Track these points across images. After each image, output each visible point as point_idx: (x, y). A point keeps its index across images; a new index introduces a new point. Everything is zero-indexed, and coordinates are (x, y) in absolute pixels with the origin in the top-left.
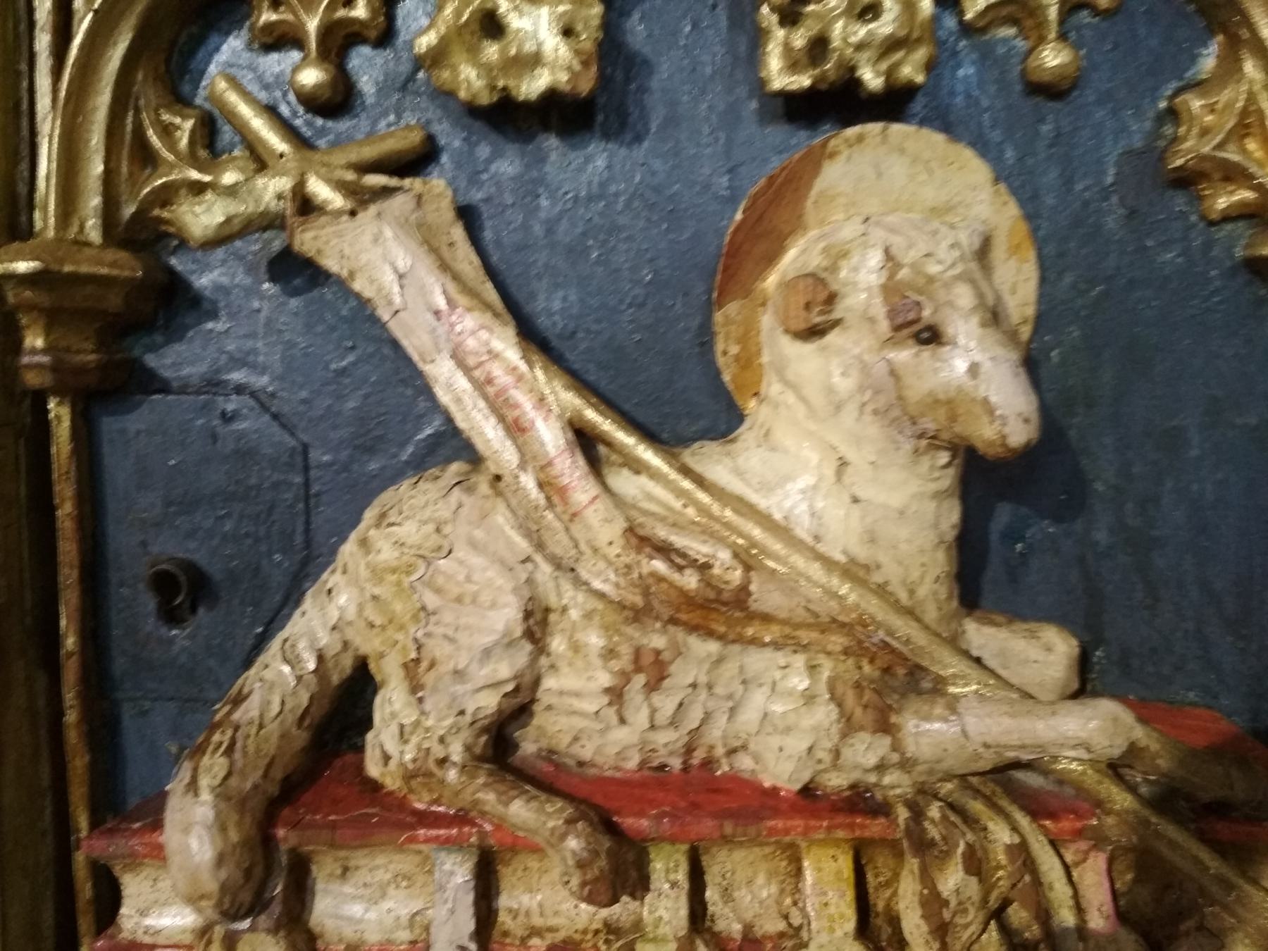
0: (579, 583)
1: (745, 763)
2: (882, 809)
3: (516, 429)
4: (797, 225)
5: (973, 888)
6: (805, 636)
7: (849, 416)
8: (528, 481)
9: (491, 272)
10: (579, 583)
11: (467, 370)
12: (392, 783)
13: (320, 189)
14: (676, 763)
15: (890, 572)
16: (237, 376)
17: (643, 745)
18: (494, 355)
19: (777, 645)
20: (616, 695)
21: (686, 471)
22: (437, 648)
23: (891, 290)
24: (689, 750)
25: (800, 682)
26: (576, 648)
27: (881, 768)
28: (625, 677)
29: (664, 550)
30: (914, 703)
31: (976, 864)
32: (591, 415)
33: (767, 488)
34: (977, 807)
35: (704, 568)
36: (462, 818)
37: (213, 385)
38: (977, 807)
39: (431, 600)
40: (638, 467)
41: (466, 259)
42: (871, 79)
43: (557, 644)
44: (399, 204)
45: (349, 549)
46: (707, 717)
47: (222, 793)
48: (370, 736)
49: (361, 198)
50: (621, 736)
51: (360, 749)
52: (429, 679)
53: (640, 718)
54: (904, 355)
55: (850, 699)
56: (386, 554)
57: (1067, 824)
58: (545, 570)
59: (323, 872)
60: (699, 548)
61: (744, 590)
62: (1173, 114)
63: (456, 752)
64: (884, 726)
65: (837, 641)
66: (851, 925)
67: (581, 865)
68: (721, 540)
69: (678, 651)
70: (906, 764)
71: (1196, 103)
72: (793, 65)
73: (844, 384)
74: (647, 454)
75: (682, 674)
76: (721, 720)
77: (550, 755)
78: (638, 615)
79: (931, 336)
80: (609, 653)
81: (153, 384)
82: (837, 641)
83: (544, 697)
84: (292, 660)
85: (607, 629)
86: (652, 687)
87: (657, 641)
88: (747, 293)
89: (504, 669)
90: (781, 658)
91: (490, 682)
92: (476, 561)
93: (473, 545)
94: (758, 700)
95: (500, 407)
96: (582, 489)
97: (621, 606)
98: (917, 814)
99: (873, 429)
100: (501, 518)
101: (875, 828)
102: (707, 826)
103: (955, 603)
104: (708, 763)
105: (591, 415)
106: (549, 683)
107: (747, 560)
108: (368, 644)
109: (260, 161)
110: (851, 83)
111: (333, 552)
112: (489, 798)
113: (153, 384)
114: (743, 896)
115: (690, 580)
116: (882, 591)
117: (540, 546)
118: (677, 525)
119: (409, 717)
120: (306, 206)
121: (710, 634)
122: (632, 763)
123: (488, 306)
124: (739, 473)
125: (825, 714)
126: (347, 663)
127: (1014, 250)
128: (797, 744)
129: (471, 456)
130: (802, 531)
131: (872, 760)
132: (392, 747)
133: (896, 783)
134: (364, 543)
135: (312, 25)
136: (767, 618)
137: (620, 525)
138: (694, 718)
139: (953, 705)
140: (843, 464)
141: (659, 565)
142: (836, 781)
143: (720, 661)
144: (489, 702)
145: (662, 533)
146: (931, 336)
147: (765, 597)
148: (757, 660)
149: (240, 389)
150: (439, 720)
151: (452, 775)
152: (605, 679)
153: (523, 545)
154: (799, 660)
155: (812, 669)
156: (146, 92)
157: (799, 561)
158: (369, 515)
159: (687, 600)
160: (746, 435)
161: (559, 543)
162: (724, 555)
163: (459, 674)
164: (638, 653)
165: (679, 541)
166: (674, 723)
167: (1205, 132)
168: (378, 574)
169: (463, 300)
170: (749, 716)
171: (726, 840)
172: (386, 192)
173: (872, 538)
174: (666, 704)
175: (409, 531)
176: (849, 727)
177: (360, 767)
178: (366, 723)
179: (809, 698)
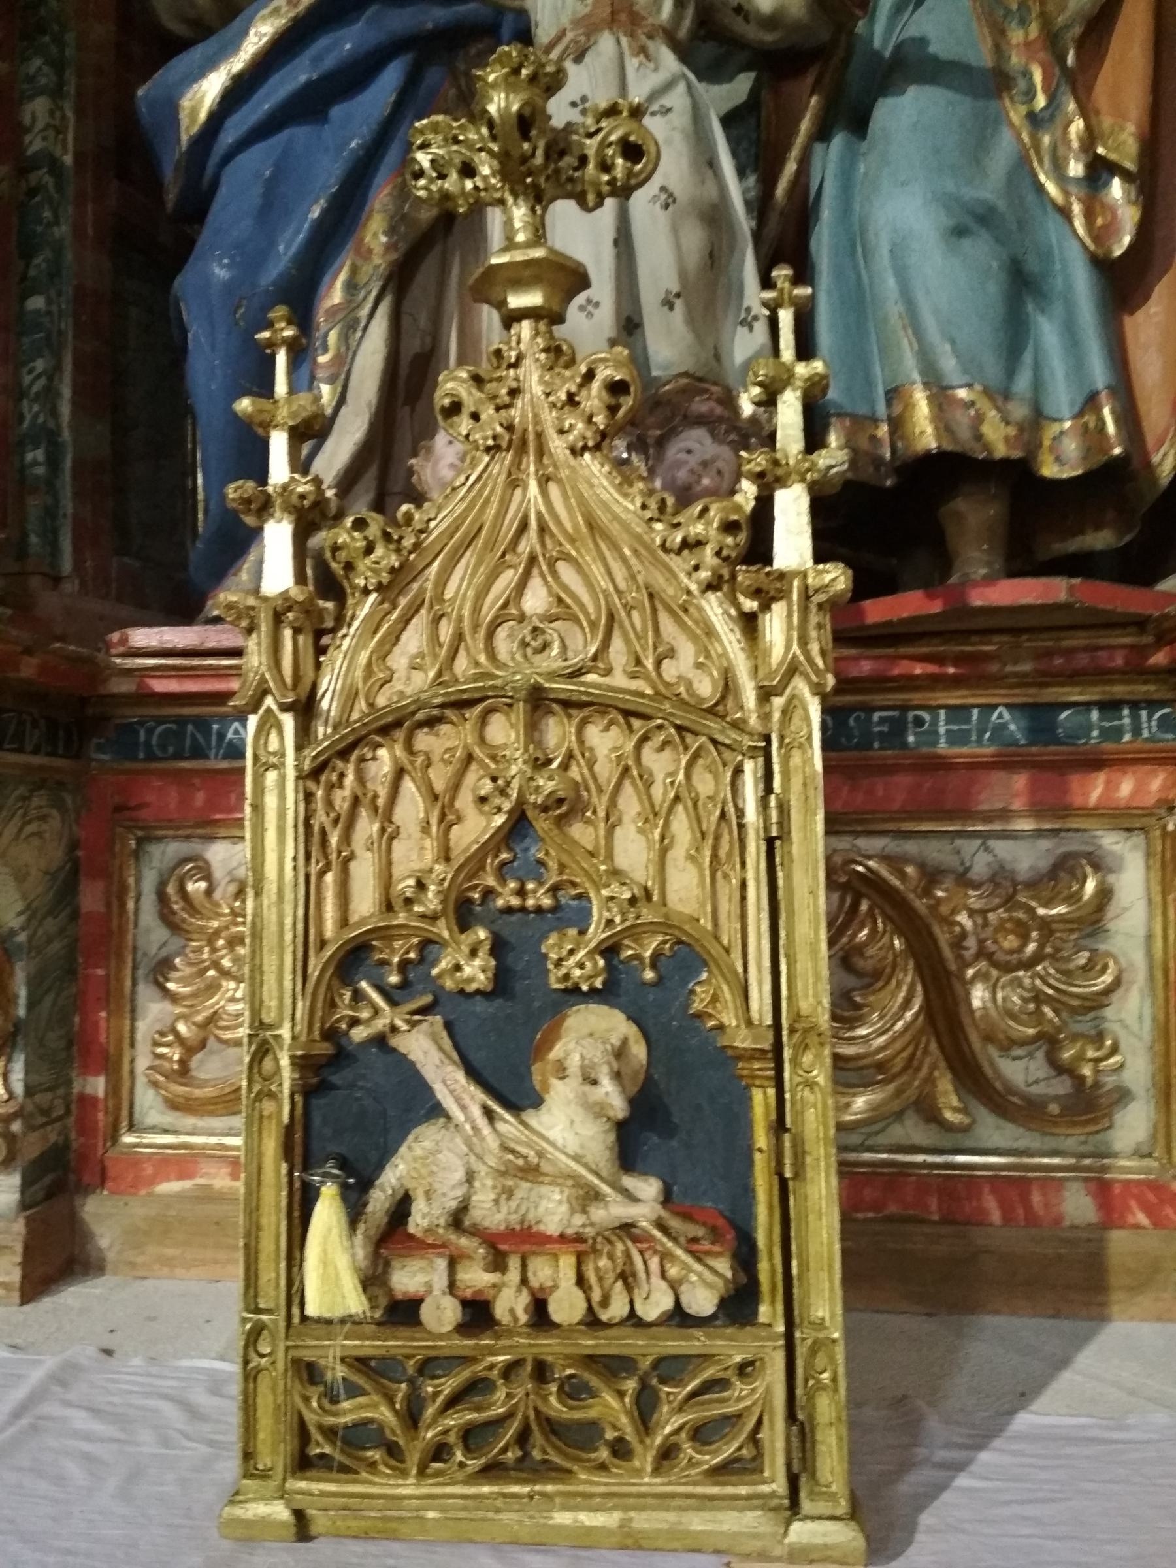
0: (485, 1163)
1: (542, 1227)
2: (584, 1241)
3: (463, 1108)
4: (558, 1038)
5: (609, 1264)
6: (560, 1181)
7: (573, 1106)
8: (468, 1127)
9: (456, 1047)
10: (485, 1163)
11: (447, 1086)
12: (419, 1235)
13: (399, 1023)
14: (518, 1227)
15: (589, 1159)
16: (360, 1083)
17: (506, 1220)
18: (456, 1081)
19: (550, 1184)
20: (496, 1202)
21: (523, 1123)
22: (437, 1186)
23: (583, 1067)
24: (522, 1222)
25: (557, 1197)
26: (483, 1185)
27: (584, 1226)
28: (499, 1195)
29: (513, 1151)
30: (595, 1204)
31: (611, 1257)
32: (490, 1103)
33: (550, 1128)
34: (614, 1238)
35: (525, 1157)
36: (443, 1246)
37: (352, 1086)
38: (614, 1238)
39: (434, 1169)
40: (506, 1121)
41: (447, 1043)
42: (585, 988)
43: (477, 1184)
44: (424, 1026)
45: (403, 1150)
46: (528, 1210)
47: (366, 1236)
48: (410, 1219)
49: (413, 1024)
50: (499, 1217)
51: (406, 1224)
52: (434, 1196)
53: (504, 1209)
54: (588, 1088)
55: (574, 1202)
56: (419, 1152)
57: (645, 1245)
58: (473, 1158)
59: (396, 1264)
60: (524, 1150)
61: (538, 1165)
62: (692, 992)
63: (442, 1222)
64: (584, 1211)
65: (570, 1182)
66: (573, 1281)
67: (484, 1258)
68: (532, 1148)
69: (517, 1186)
70: (592, 1224)
71: (698, 989)
72: (559, 981)
73: (571, 1096)
74: (508, 1117)
75: (519, 1194)
76: (532, 1210)
77: (474, 1225)
78: (504, 1174)
79: (595, 1082)
80: (494, 1187)
81: (333, 1087)
82: (570, 1182)
83: (473, 1204)
84: (384, 1191)
85: (494, 1179)
86: (509, 1199)
87: (510, 1183)
88: (542, 1059)
89: (459, 1192)
90: (552, 1188)
91: (741, 993)
92: (450, 1155)
93: (450, 1150)
94: (544, 1204)
95: (458, 1100)
96: (486, 1130)
97: (498, 1171)
98: (594, 1240)
99: (581, 1111)
100: (458, 1140)
101: (582, 1247)
102: (526, 1248)
103: (616, 1168)
104: (530, 1227)
105: (490, 1103)
106: (474, 1198)
107: (541, 1154)
108: (410, 1185)
109: (377, 1012)
110: (576, 989)
111: (396, 1151)
112: (453, 1237)
113: (333, 1087)
114: (540, 1274)
115: (520, 1162)
116: (586, 1166)
117: (471, 1150)
118: (518, 1142)
119: (426, 1210)
120: (394, 1029)
121: (527, 1180)
122: (502, 1227)
123: (454, 1062)
124: (540, 1123)
125: (564, 1208)
126: (402, 1192)
127: (637, 1042)
128: (557, 1218)
129: (448, 1117)
130: (560, 1143)
131: (580, 1223)
132: (419, 1221)
133: (589, 1232)
134: (410, 1148)
135: (396, 960)
136: (546, 1175)
137: (498, 1143)
138: (523, 1211)
139: (606, 1204)
140: (572, 1122)
141: (510, 1157)
142: (570, 1231)
143: (531, 1190)
144: (453, 1204)
145: (512, 1145)
146: (595, 1082)
147: (545, 1167)
148: (544, 1190)
149: (362, 1088)
150: (436, 1211)
151: (441, 1231)
152: (493, 1196)
153: (465, 1149)
154: (557, 1189)
155: (562, 1192)
156: (336, 983)
157: (557, 1154)
158: (411, 1137)
159: (521, 1169)
160: (544, 1108)
161: (478, 1150)
162: (532, 1153)
163: (444, 1194)
164: (504, 1187)
165: (518, 1148)
166: (516, 1212)
167: (702, 1000)
168: (415, 1159)
169: (447, 1061)
170: (541, 1209)
171: (534, 1253)
172: (420, 1022)
173: (582, 1146)
174: (513, 1204)
175: (427, 1144)
176: (573, 1211)
177: (406, 1230)
178: (409, 1214)
179: (560, 1202)
